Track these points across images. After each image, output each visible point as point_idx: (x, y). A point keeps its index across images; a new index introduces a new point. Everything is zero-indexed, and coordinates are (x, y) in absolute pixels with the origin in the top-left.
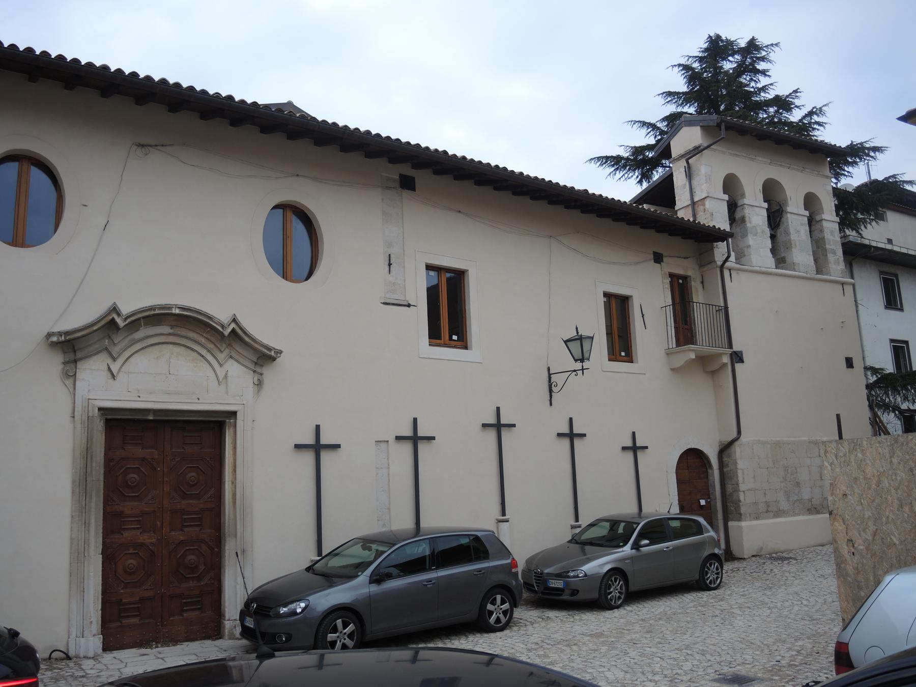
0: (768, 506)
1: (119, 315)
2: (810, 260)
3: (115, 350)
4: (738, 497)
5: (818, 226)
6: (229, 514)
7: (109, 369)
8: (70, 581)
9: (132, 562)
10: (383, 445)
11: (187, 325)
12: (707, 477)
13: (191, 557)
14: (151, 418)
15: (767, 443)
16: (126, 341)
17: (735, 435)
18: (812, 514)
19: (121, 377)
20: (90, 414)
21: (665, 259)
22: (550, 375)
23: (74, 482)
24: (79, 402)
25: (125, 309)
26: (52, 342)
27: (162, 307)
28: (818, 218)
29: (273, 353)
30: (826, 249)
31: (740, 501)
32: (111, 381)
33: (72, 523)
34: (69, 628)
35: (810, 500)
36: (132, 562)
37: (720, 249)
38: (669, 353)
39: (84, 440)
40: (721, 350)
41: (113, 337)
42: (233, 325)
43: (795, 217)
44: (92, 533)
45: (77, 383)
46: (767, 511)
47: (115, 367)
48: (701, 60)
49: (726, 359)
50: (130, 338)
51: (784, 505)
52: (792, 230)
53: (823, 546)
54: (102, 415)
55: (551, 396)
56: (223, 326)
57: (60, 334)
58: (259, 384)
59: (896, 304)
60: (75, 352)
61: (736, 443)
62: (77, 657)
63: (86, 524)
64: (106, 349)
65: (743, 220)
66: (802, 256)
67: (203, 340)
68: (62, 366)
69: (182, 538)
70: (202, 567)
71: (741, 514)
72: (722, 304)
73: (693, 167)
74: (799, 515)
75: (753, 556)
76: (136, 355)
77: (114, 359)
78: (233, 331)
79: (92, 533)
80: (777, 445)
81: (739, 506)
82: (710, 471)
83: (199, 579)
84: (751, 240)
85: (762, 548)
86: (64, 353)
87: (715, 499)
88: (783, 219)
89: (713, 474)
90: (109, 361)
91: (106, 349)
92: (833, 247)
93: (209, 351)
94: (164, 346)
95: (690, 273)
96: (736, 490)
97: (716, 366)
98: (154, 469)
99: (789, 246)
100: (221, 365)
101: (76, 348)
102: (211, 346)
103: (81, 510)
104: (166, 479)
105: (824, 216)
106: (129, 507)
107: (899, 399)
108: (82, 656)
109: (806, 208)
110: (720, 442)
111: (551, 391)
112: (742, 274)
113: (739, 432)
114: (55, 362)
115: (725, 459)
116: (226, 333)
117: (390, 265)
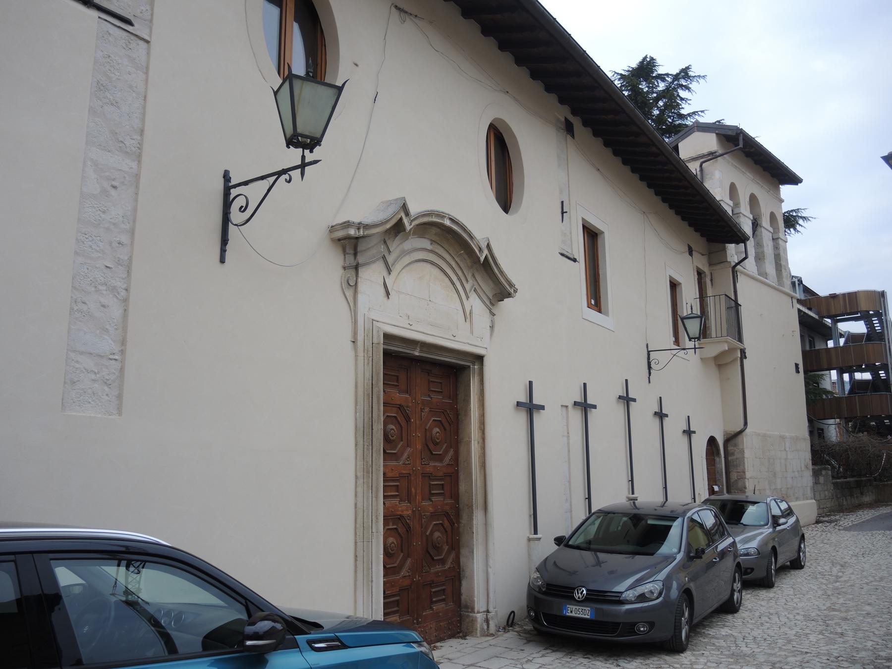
1: (407, 214)
3: (390, 260)
4: (744, 483)
8: (356, 566)
10: (564, 409)
13: (437, 534)
17: (741, 426)
20: (375, 341)
22: (649, 352)
25: (415, 208)
29: (512, 291)
37: (733, 251)
41: (388, 242)
45: (360, 297)
48: (622, 77)
55: (650, 374)
60: (355, 255)
61: (744, 433)
64: (384, 258)
68: (342, 271)
90: (385, 273)
93: (459, 279)
98: (408, 419)
100: (468, 297)
101: (359, 249)
111: (650, 367)
113: (746, 423)
114: (332, 264)
115: (730, 448)
117: (563, 213)
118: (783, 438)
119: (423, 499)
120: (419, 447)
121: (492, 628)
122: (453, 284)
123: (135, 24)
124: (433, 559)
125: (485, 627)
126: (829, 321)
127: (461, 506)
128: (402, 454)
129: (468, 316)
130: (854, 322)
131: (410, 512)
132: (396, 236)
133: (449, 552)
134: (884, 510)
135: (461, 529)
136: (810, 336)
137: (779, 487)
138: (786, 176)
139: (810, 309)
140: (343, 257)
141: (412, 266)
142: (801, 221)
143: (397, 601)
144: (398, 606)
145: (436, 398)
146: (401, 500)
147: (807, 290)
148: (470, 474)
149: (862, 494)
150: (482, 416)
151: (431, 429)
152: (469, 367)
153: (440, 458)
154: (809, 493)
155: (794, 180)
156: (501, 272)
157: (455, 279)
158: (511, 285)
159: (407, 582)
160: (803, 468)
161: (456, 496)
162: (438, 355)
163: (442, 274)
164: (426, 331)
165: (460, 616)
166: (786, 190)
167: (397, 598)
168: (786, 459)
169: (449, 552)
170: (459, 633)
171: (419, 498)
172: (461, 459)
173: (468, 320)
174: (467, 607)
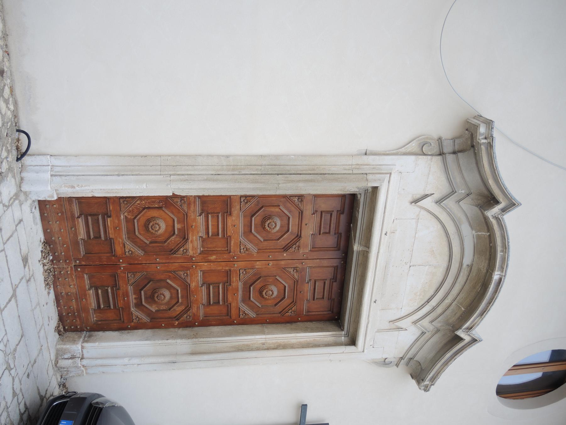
1: (504, 210)
3: (450, 203)
6: (223, 342)
7: (426, 196)
8: (135, 156)
9: (162, 227)
11: (476, 285)
13: (167, 294)
14: (356, 247)
16: (459, 215)
19: (415, 209)
20: (370, 177)
23: (277, 157)
24: (387, 160)
25: (509, 219)
26: (476, 127)
27: (504, 260)
29: (427, 382)
32: (410, 199)
33: (219, 156)
34: (66, 156)
36: (162, 227)
39: (334, 170)
41: (468, 200)
42: (467, 339)
44: (203, 185)
45: (413, 158)
47: (428, 203)
50: (464, 219)
54: (366, 191)
56: (470, 329)
57: (490, 138)
58: (385, 363)
60: (454, 153)
62: (22, 169)
63: (216, 176)
64: (453, 192)
67: (448, 301)
68: (436, 136)
69: (193, 285)
70: (153, 308)
76: (439, 226)
77: (439, 202)
78: (460, 339)
79: (203, 185)
83: (139, 305)
86: (454, 139)
90: (437, 196)
91: (453, 192)
93: (434, 309)
94: (447, 258)
98: (286, 248)
100: (415, 323)
102: (439, 310)
103: (236, 167)
104: (271, 263)
106: (237, 221)
108: (24, 174)
116: (460, 333)
119: (204, 272)
120: (258, 265)
121: (62, 363)
122: (428, 301)
123: (483, 338)
124: (142, 289)
125: (66, 356)
127: (196, 329)
128: (251, 241)
129: (395, 325)
131: (191, 253)
132: (477, 206)
133: (149, 313)
135: (172, 329)
140: (450, 138)
141: (445, 239)
143: (100, 237)
144: (95, 238)
145: (307, 289)
146: (203, 240)
148: (230, 335)
150: (292, 346)
151: (276, 282)
152: (343, 330)
153: (246, 299)
156: (447, 363)
157: (433, 303)
158: (433, 380)
159: (118, 250)
161: (205, 323)
162: (356, 272)
163: (438, 285)
164: (380, 254)
165: (82, 330)
167: (103, 238)
169: (149, 313)
170: (64, 328)
171: (205, 266)
172: (245, 327)
173: (393, 326)
174: (90, 336)
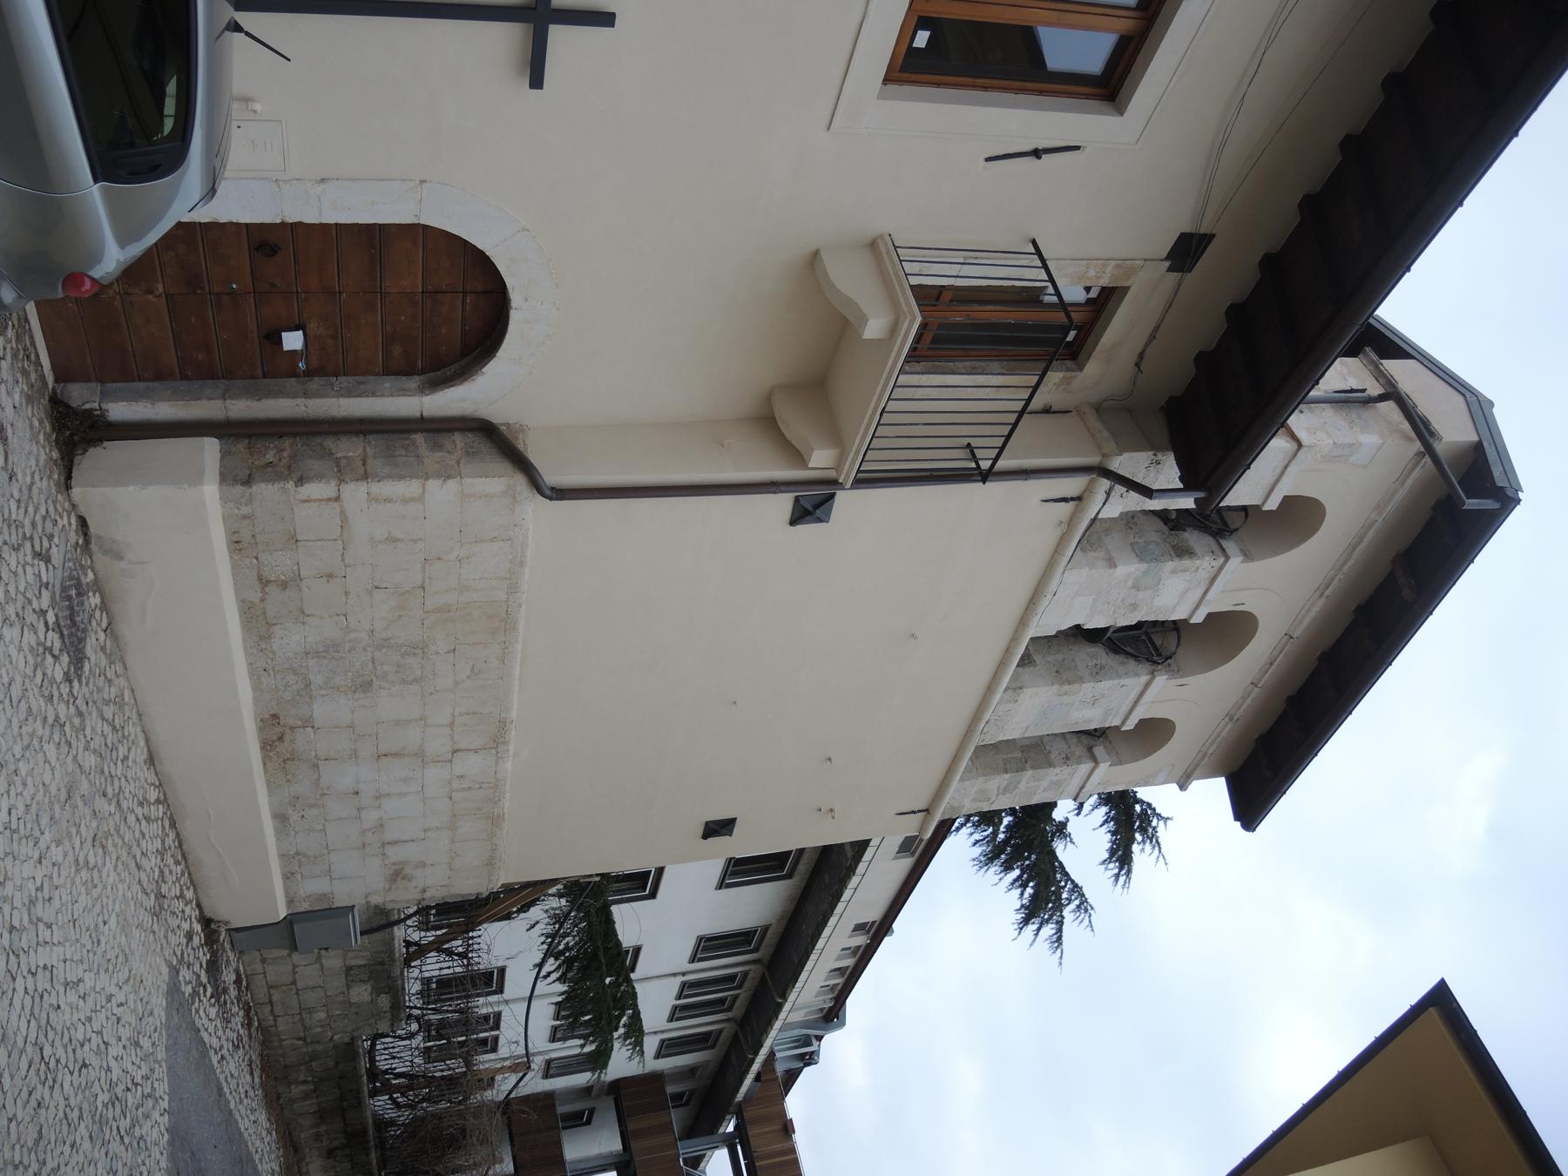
0: (284, 585)
2: (1012, 731)
4: (319, 477)
5: (1079, 751)
12: (388, 371)
15: (513, 589)
17: (551, 478)
18: (261, 730)
21: (1174, 276)
28: (1099, 751)
30: (1021, 769)
31: (301, 481)
35: (308, 723)
38: (876, 248)
40: (857, 445)
43: (1138, 689)
46: (264, 582)
49: (821, 460)
51: (290, 640)
52: (1105, 685)
53: (151, 760)
59: (734, 874)
61: (520, 481)
65: (1182, 552)
66: (1037, 708)
71: (248, 482)
72: (1002, 464)
73: (1367, 414)
74: (257, 687)
75: (83, 523)
80: (502, 622)
81: (279, 477)
82: (413, 382)
84: (1128, 569)
85: (119, 556)
87: (306, 395)
88: (1132, 664)
89: (404, 392)
92: (1022, 786)
95: (1093, 368)
96: (342, 472)
97: (795, 426)
99: (1063, 675)
105: (1104, 767)
107: (554, 903)
109: (1144, 724)
110: (522, 429)
112: (1049, 537)
113: (560, 494)
118: (497, 742)
126: (731, 1128)
130: (887, 941)
134: (254, 1126)
136: (692, 1092)
137: (321, 710)
138: (1252, 798)
139: (758, 1078)
142: (1048, 930)
147: (791, 1077)
149: (330, 1153)
154: (313, 888)
155: (1250, 806)
160: (395, 854)
166: (1214, 793)
168: (420, 755)
